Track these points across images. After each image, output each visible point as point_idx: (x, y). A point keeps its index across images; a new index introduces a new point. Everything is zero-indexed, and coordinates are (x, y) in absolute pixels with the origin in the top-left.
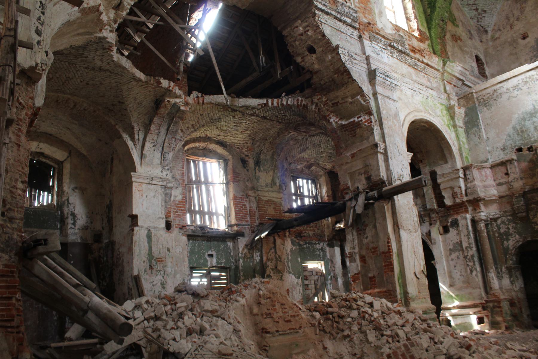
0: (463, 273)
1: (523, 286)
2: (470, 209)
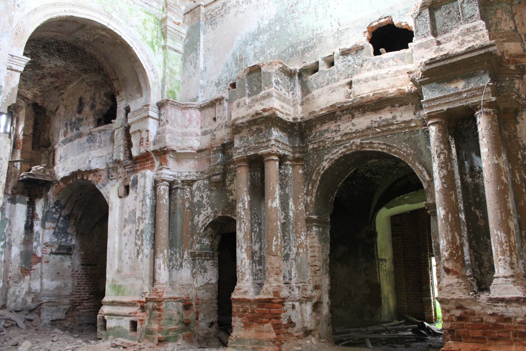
0: (132, 256)
1: (214, 281)
2: (157, 164)
